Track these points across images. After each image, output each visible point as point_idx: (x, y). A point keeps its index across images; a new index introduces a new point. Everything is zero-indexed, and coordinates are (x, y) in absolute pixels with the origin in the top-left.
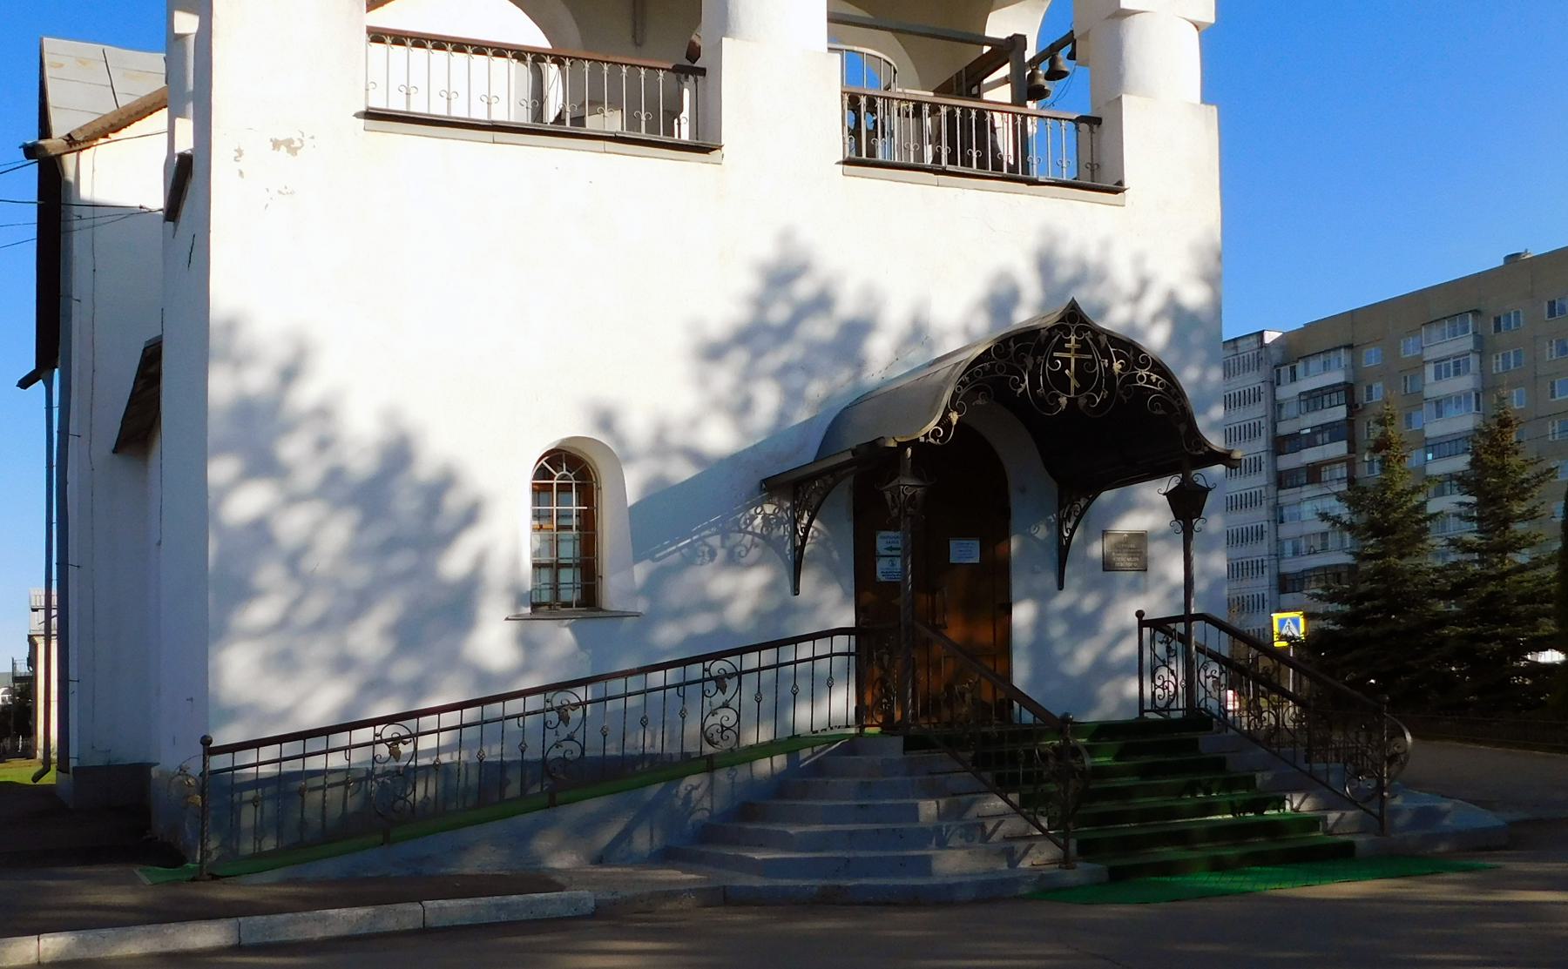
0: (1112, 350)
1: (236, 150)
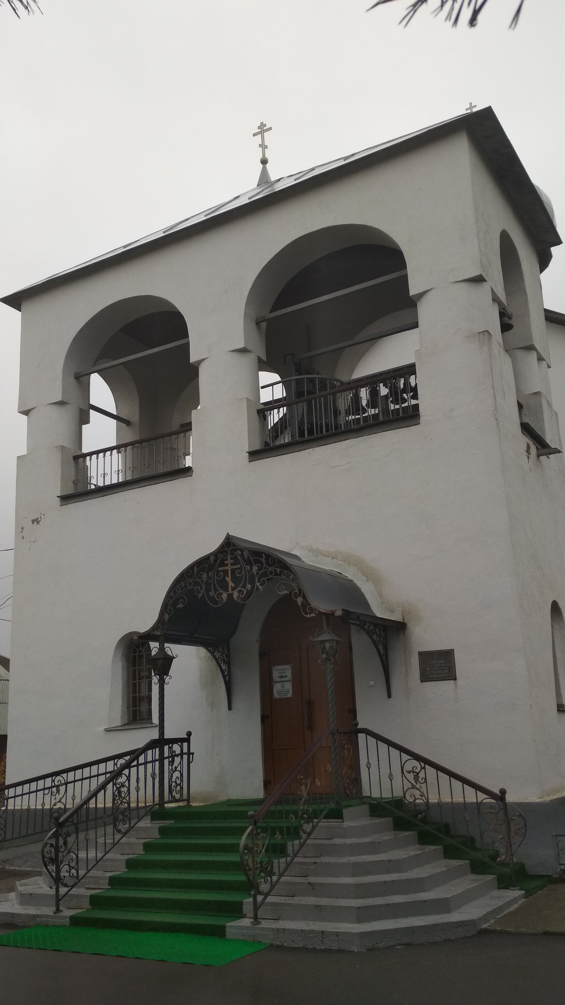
0: (252, 559)
1: (22, 528)
